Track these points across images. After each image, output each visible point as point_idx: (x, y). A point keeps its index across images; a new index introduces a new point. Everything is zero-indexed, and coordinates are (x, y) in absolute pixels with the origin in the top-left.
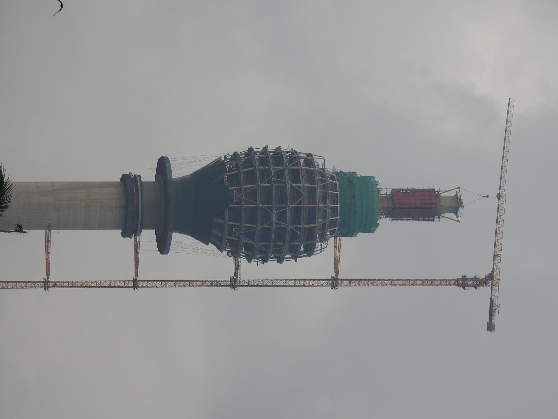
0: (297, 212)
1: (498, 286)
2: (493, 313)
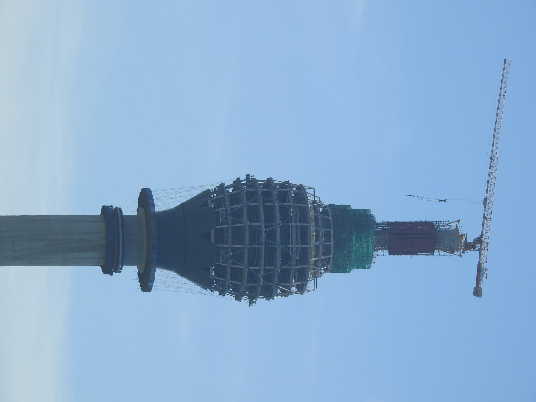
1: (487, 250)
2: (481, 278)
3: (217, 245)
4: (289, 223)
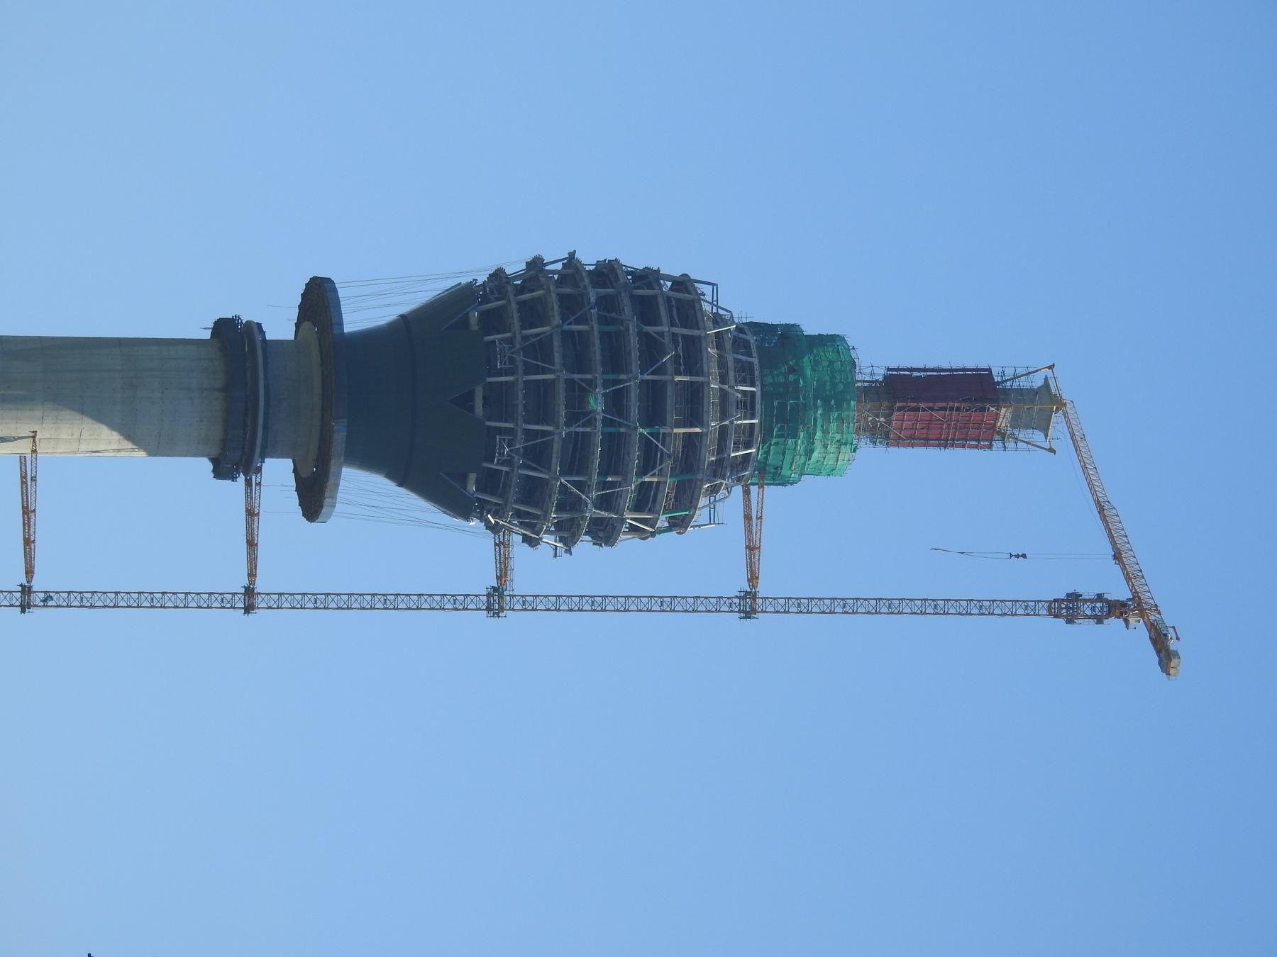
0: (654, 394)
3: (488, 423)
4: (657, 482)
